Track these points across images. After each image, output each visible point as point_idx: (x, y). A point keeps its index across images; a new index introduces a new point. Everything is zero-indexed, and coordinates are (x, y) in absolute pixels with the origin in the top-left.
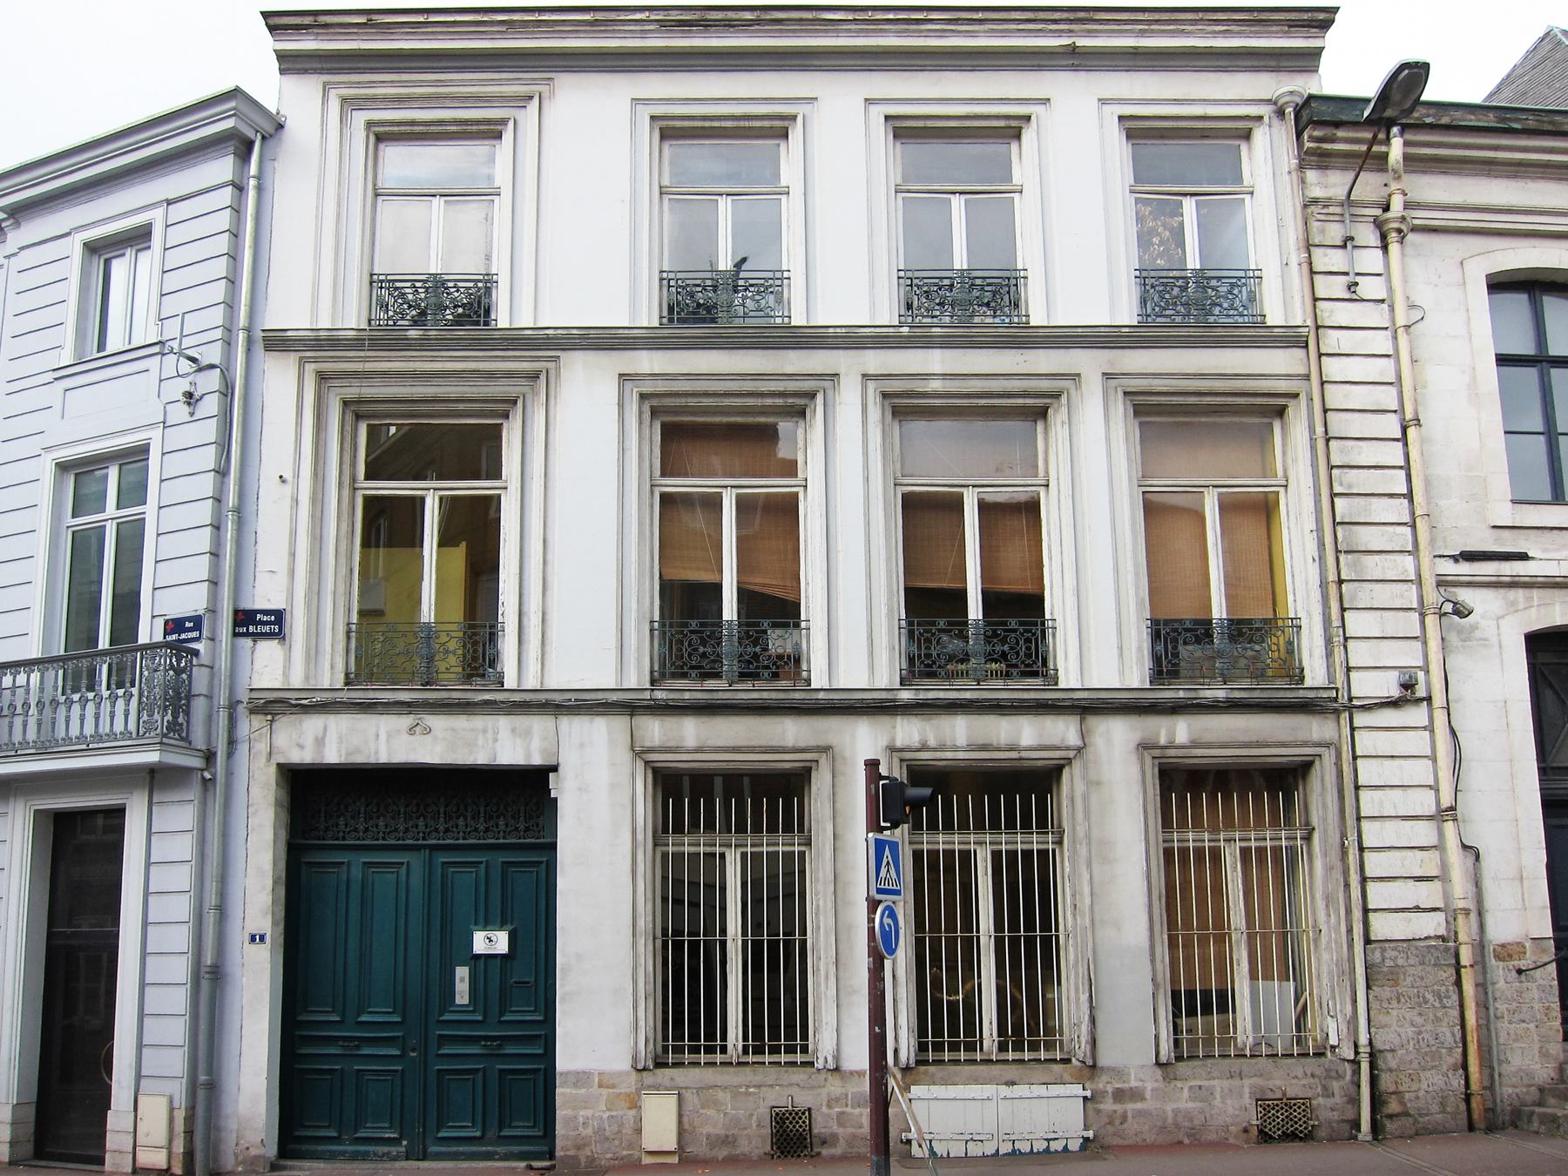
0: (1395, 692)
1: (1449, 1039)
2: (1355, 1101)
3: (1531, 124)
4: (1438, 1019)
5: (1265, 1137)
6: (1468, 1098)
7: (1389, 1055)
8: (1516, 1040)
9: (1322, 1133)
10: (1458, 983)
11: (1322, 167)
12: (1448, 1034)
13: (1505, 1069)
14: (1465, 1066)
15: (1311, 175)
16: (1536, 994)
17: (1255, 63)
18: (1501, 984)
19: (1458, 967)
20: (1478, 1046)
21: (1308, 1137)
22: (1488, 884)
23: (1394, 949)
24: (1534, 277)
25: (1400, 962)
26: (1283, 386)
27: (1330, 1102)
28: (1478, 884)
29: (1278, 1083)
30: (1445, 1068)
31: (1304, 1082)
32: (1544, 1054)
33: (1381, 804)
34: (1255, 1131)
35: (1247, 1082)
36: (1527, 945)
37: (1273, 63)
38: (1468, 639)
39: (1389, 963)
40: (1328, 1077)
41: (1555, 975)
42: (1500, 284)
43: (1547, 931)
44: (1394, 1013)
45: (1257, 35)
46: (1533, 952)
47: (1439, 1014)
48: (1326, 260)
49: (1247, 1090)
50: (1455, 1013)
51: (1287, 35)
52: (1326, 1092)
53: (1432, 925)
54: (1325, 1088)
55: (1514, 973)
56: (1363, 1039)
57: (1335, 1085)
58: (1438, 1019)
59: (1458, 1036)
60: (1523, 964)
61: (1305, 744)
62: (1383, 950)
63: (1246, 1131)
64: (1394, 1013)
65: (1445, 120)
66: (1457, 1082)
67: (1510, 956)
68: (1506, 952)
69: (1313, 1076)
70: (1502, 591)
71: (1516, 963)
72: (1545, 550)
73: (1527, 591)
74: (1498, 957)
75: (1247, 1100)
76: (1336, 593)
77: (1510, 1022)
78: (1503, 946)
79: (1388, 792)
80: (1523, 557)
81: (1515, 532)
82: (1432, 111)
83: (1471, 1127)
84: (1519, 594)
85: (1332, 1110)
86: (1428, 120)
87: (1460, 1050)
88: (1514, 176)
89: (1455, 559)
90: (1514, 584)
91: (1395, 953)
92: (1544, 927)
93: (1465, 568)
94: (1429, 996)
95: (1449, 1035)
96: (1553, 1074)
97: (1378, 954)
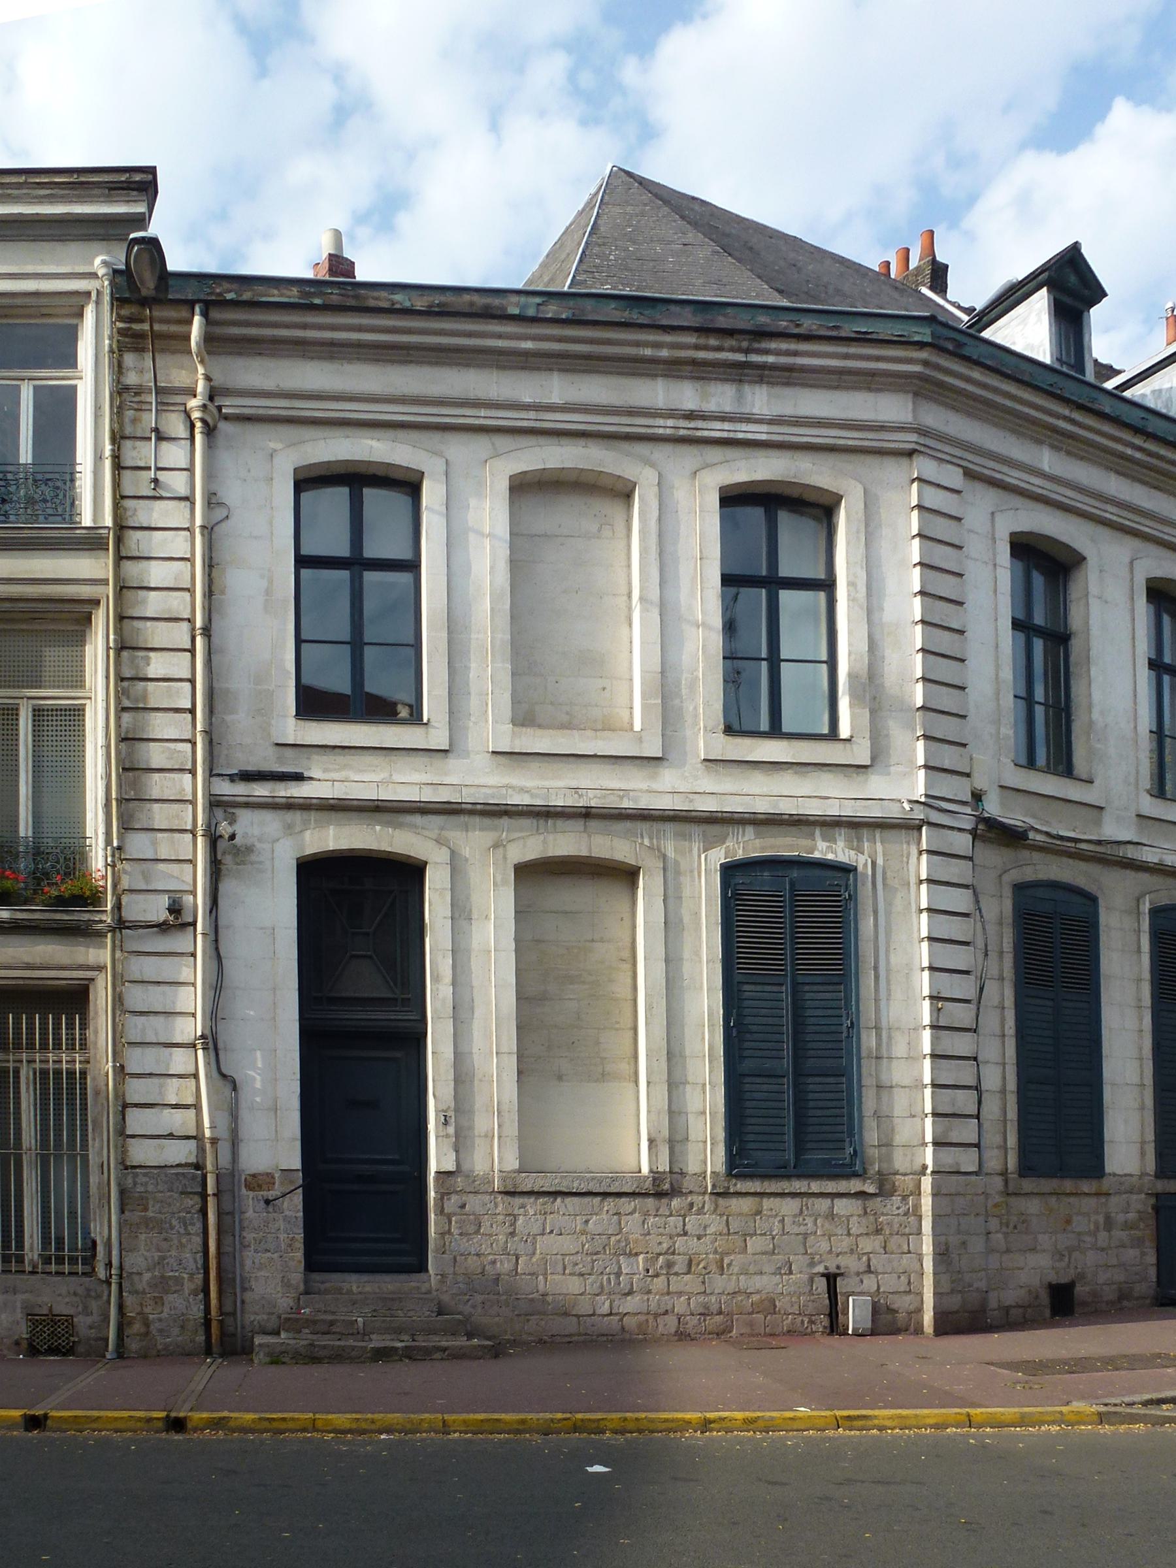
0: (163, 915)
1: (192, 1266)
2: (106, 1319)
3: (335, 299)
4: (182, 1246)
5: (33, 1351)
6: (207, 1323)
7: (136, 1278)
8: (260, 1269)
9: (81, 1349)
10: (204, 1212)
11: (140, 350)
12: (191, 1260)
13: (248, 1296)
14: (206, 1290)
15: (129, 359)
16: (281, 1224)
17: (86, 231)
18: (250, 1214)
19: (204, 1196)
20: (224, 1276)
21: (69, 1351)
22: (245, 1115)
23: (145, 1175)
24: (351, 470)
25: (150, 1188)
26: (85, 591)
27: (89, 1320)
28: (234, 1115)
29: (45, 1299)
30: (187, 1292)
31: (67, 1300)
32: (286, 1284)
33: (144, 1030)
34: (24, 1344)
35: (20, 1297)
36: (277, 1176)
37: (102, 231)
38: (243, 863)
39: (140, 1189)
40: (88, 1296)
41: (301, 1207)
42: (308, 481)
43: (296, 1164)
44: (143, 1237)
45: (80, 200)
46: (282, 1183)
47: (184, 1241)
48: (134, 453)
49: (19, 1305)
50: (198, 1240)
51: (109, 200)
52: (87, 1312)
53: (181, 1153)
54: (85, 1307)
55: (262, 1203)
56: (115, 1261)
57: (94, 1305)
58: (182, 1246)
59: (200, 1262)
60: (271, 1194)
61: (80, 967)
62: (136, 1175)
63: (17, 1343)
64: (143, 1237)
65: (247, 296)
66: (197, 1311)
67: (260, 1186)
68: (257, 1182)
69: (75, 1294)
70: (281, 813)
71: (265, 1193)
72: (325, 770)
73: (305, 814)
74: (249, 1187)
75: (19, 1315)
76: (129, 805)
77: (256, 1251)
78: (254, 1176)
79: (151, 1018)
80: (298, 777)
81: (297, 750)
82: (235, 286)
83: (208, 1352)
84: (297, 817)
85: (91, 1328)
86: (229, 296)
87: (201, 1276)
88: (331, 358)
89: (232, 778)
90: (290, 805)
91: (144, 1179)
92: (293, 1160)
93: (240, 789)
94: (174, 1222)
95: (192, 1260)
96: (292, 1304)
97: (130, 1181)
